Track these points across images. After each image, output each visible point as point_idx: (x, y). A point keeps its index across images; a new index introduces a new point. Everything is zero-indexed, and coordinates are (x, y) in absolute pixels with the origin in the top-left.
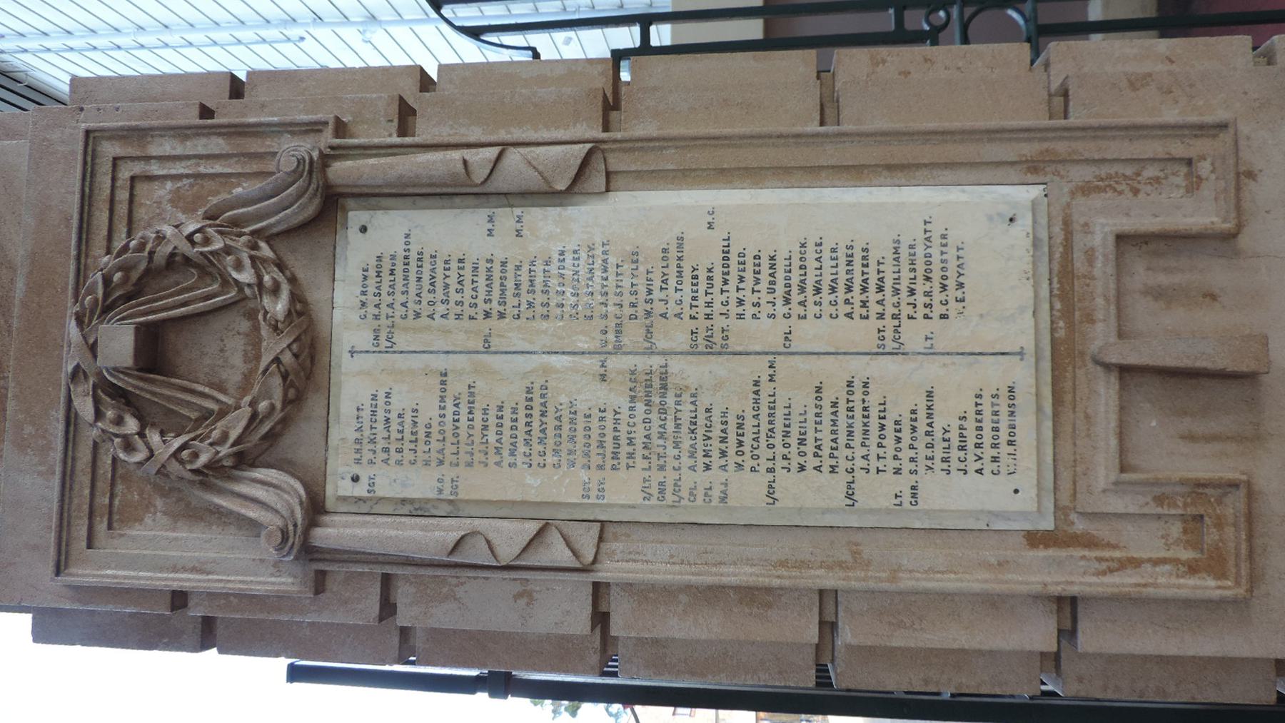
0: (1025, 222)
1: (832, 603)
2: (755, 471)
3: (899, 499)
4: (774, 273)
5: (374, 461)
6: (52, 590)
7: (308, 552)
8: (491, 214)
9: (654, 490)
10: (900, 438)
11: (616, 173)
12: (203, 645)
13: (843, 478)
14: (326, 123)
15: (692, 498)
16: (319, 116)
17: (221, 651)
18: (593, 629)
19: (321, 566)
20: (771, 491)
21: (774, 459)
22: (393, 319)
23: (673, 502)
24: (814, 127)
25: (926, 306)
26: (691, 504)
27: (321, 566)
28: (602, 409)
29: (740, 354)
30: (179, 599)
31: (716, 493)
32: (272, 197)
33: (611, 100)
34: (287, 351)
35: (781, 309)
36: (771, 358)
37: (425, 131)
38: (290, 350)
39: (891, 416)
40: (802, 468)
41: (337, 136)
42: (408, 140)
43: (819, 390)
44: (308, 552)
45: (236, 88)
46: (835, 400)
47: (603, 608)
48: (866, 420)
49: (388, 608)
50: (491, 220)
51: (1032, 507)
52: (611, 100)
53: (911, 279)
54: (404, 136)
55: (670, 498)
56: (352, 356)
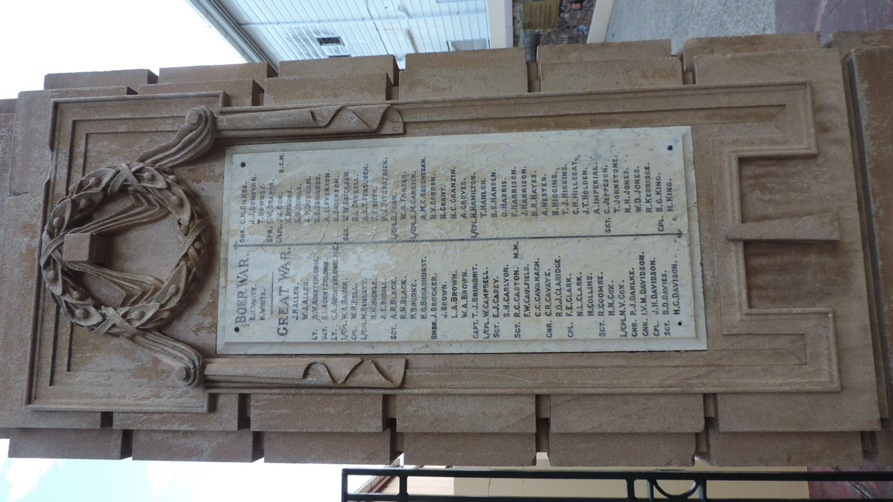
0: (678, 147)
1: (712, 403)
2: (413, 318)
3: (315, 335)
4: (454, 190)
5: (635, 312)
6: (22, 417)
7: (206, 382)
8: (281, 155)
9: (629, 330)
10: (446, 292)
11: (409, 123)
12: (255, 456)
13: (469, 321)
14: (217, 96)
15: (570, 334)
16: (215, 92)
17: (266, 461)
18: (384, 430)
19: (215, 391)
20: (486, 329)
21: (582, 307)
22: (588, 207)
23: (621, 336)
24: (526, 93)
25: (492, 208)
26: (655, 337)
27: (215, 391)
28: (547, 273)
29: (566, 237)
30: (107, 418)
31: (492, 331)
32: (178, 143)
33: (392, 80)
34: (57, 250)
35: (603, 207)
36: (514, 242)
37: (268, 101)
38: (193, 246)
39: (659, 273)
40: (465, 315)
41: (253, 105)
42: (228, 109)
43: (642, 257)
44: (206, 382)
45: (151, 78)
46: (675, 263)
47: (545, 415)
48: (632, 276)
49: (244, 421)
50: (281, 158)
51: (691, 333)
52: (392, 80)
53: (574, 189)
54: (227, 106)
55: (482, 335)
56: (236, 249)
